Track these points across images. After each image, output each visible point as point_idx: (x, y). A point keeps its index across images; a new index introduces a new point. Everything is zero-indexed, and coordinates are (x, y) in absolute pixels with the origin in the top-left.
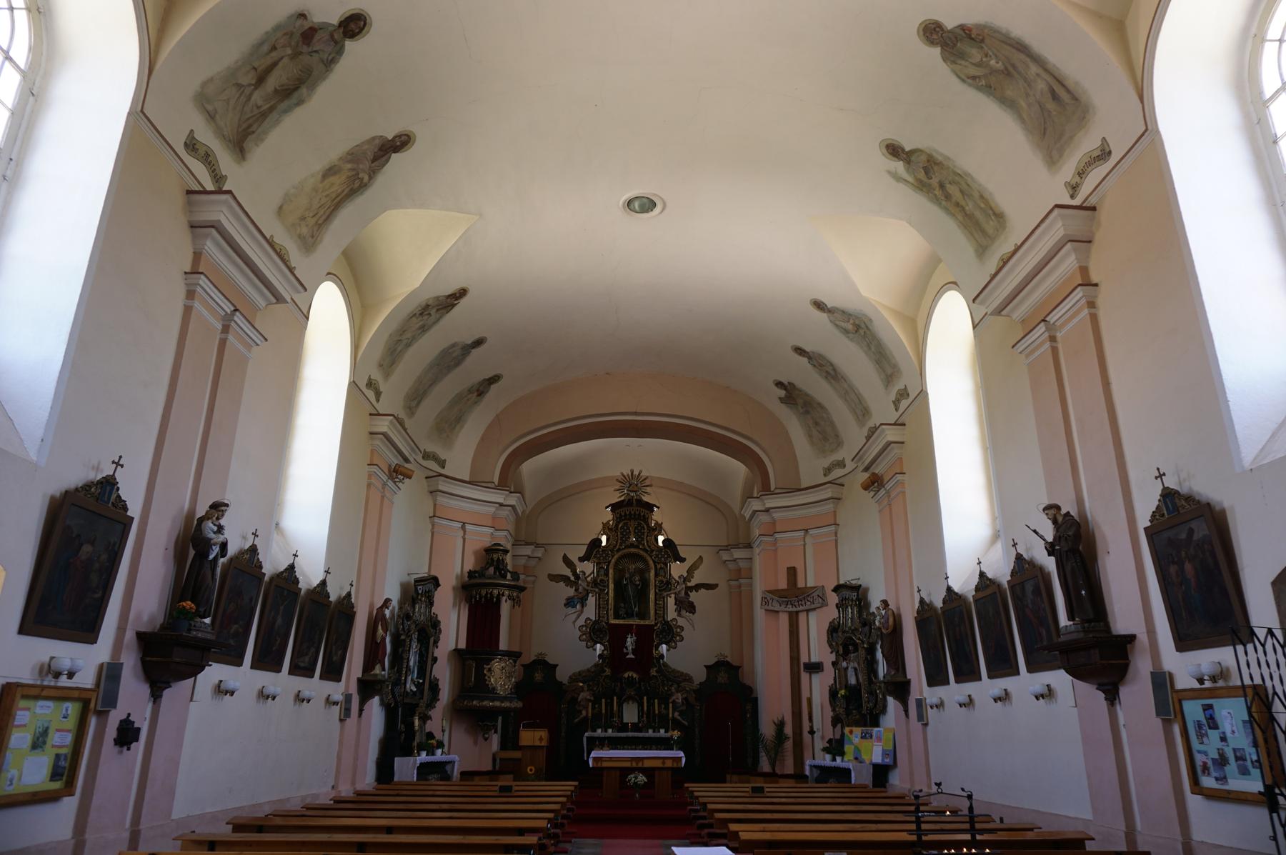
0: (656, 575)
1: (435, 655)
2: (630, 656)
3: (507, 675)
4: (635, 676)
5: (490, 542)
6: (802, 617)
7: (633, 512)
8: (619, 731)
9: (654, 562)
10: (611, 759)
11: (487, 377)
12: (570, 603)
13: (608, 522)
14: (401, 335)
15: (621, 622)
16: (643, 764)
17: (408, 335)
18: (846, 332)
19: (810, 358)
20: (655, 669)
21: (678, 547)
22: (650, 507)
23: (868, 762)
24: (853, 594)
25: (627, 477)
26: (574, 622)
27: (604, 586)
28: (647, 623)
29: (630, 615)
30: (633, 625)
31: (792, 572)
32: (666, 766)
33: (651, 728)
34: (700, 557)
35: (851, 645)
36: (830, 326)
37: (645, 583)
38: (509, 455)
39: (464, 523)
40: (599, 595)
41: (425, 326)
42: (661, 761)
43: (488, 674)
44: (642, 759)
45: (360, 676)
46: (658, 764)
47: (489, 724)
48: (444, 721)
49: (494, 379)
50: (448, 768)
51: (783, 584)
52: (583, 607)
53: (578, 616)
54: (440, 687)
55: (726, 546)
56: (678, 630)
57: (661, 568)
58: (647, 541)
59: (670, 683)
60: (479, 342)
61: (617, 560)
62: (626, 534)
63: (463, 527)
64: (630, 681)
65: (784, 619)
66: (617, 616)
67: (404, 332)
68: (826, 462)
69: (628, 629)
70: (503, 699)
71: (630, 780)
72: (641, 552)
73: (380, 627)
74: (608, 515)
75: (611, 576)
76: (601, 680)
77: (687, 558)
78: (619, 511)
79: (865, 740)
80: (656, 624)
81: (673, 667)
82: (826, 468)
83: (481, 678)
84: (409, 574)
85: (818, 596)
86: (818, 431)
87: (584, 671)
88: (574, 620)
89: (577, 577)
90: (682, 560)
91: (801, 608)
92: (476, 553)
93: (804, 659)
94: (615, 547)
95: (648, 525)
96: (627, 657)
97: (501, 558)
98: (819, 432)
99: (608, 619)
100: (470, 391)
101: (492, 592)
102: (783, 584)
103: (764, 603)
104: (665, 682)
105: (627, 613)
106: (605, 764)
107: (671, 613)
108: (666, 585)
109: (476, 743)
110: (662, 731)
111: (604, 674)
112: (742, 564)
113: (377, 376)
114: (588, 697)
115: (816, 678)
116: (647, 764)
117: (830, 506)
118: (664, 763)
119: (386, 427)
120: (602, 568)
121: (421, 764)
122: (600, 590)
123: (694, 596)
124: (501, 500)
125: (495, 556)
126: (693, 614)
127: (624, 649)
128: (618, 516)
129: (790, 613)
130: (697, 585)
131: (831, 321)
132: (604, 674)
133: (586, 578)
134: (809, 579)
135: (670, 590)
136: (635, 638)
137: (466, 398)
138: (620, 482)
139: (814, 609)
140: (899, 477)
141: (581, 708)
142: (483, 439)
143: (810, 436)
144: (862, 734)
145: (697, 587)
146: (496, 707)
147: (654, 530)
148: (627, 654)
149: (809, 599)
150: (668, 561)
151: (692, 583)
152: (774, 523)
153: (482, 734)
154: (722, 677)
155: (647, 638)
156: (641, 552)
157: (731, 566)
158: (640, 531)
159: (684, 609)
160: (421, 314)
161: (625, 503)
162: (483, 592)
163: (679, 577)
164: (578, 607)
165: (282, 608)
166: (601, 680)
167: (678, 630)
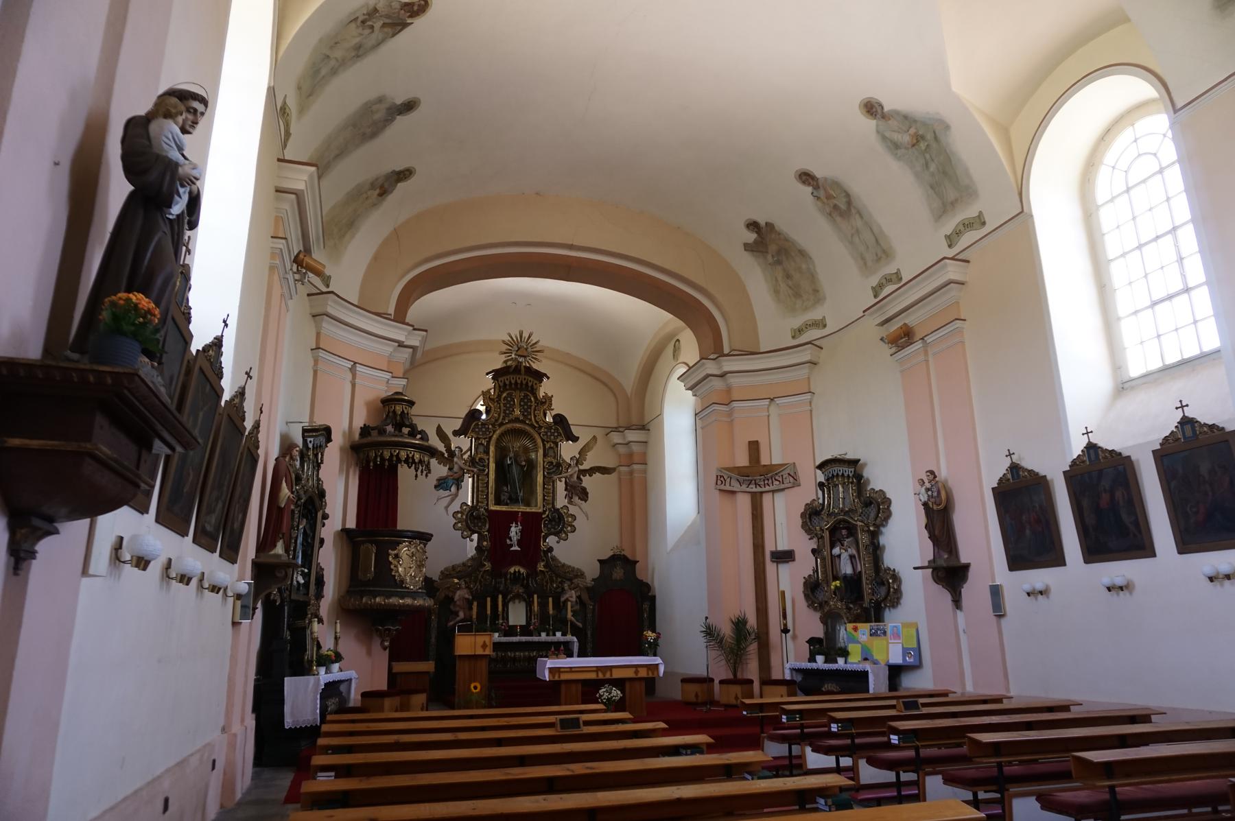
0: (545, 455)
1: (321, 537)
2: (516, 548)
3: (418, 563)
4: (522, 570)
5: (386, 391)
6: (767, 499)
7: (519, 382)
8: (505, 635)
9: (543, 441)
10: (571, 670)
11: (398, 169)
12: (441, 484)
13: (488, 391)
14: (331, 48)
15: (504, 508)
16: (611, 675)
17: (338, 53)
18: (894, 147)
19: (817, 187)
20: (542, 564)
21: (571, 426)
22: (539, 376)
23: (883, 663)
24: (850, 470)
25: (515, 339)
26: (446, 508)
27: (484, 466)
28: (533, 510)
29: (514, 500)
30: (519, 512)
31: (754, 447)
32: (640, 675)
33: (544, 631)
34: (594, 437)
35: (843, 528)
36: (873, 139)
37: (532, 465)
38: (406, 286)
39: (355, 363)
40: (478, 476)
41: (360, 47)
42: (634, 669)
43: (395, 562)
44: (611, 668)
45: (254, 557)
46: (630, 674)
47: (391, 628)
48: (338, 625)
49: (403, 175)
50: (343, 688)
51: (742, 460)
52: (458, 489)
53: (452, 500)
54: (325, 579)
55: (616, 428)
56: (570, 519)
57: (550, 448)
58: (535, 416)
59: (559, 580)
60: (409, 106)
61: (500, 436)
62: (510, 407)
63: (353, 370)
64: (517, 577)
65: (744, 502)
66: (498, 502)
67: (336, 43)
68: (797, 322)
69: (512, 517)
70: (413, 595)
71: (601, 696)
72: (527, 428)
73: (284, 484)
74: (488, 383)
75: (491, 454)
76: (480, 577)
77: (580, 436)
78: (502, 379)
79: (874, 638)
80: (544, 512)
81: (563, 561)
82: (795, 330)
83: (384, 566)
84: (287, 423)
85: (789, 474)
86: (788, 285)
87: (459, 566)
88: (445, 505)
89: (452, 454)
90: (575, 439)
91: (767, 488)
92: (369, 405)
93: (769, 547)
94: (496, 421)
95: (536, 398)
96: (512, 549)
97: (406, 412)
98: (790, 287)
99: (487, 505)
100: (373, 186)
101: (382, 454)
102: (742, 460)
103: (719, 482)
104: (554, 578)
105: (510, 498)
106: (564, 677)
107: (561, 501)
108: (556, 467)
109: (369, 653)
110: (559, 634)
111: (483, 569)
112: (636, 448)
113: (292, 104)
114: (467, 596)
115: (785, 570)
116: (617, 674)
117: (803, 372)
118: (636, 672)
119: (304, 183)
120: (482, 444)
121: (326, 684)
122: (479, 470)
123: (587, 481)
124: (402, 338)
125: (399, 409)
126: (586, 501)
127: (508, 541)
128: (501, 384)
129: (753, 494)
130: (591, 468)
131: (878, 132)
132: (483, 569)
133: (462, 455)
134: (774, 455)
135: (560, 474)
136: (521, 527)
137: (365, 196)
138: (508, 344)
139: (783, 490)
140: (958, 324)
141: (457, 609)
142: (376, 257)
143: (776, 292)
144: (871, 630)
145: (592, 471)
146: (408, 605)
147: (543, 403)
148: (511, 546)
149: (777, 478)
150: (558, 440)
151: (586, 466)
152: (729, 390)
153: (379, 641)
154: (618, 573)
155: (533, 527)
156: (527, 428)
157: (622, 450)
158: (526, 404)
159: (577, 495)
160: (363, 22)
161: (511, 370)
162: (387, 454)
163: (571, 459)
164: (453, 489)
165: (201, 414)
166: (480, 577)
167: (570, 519)
